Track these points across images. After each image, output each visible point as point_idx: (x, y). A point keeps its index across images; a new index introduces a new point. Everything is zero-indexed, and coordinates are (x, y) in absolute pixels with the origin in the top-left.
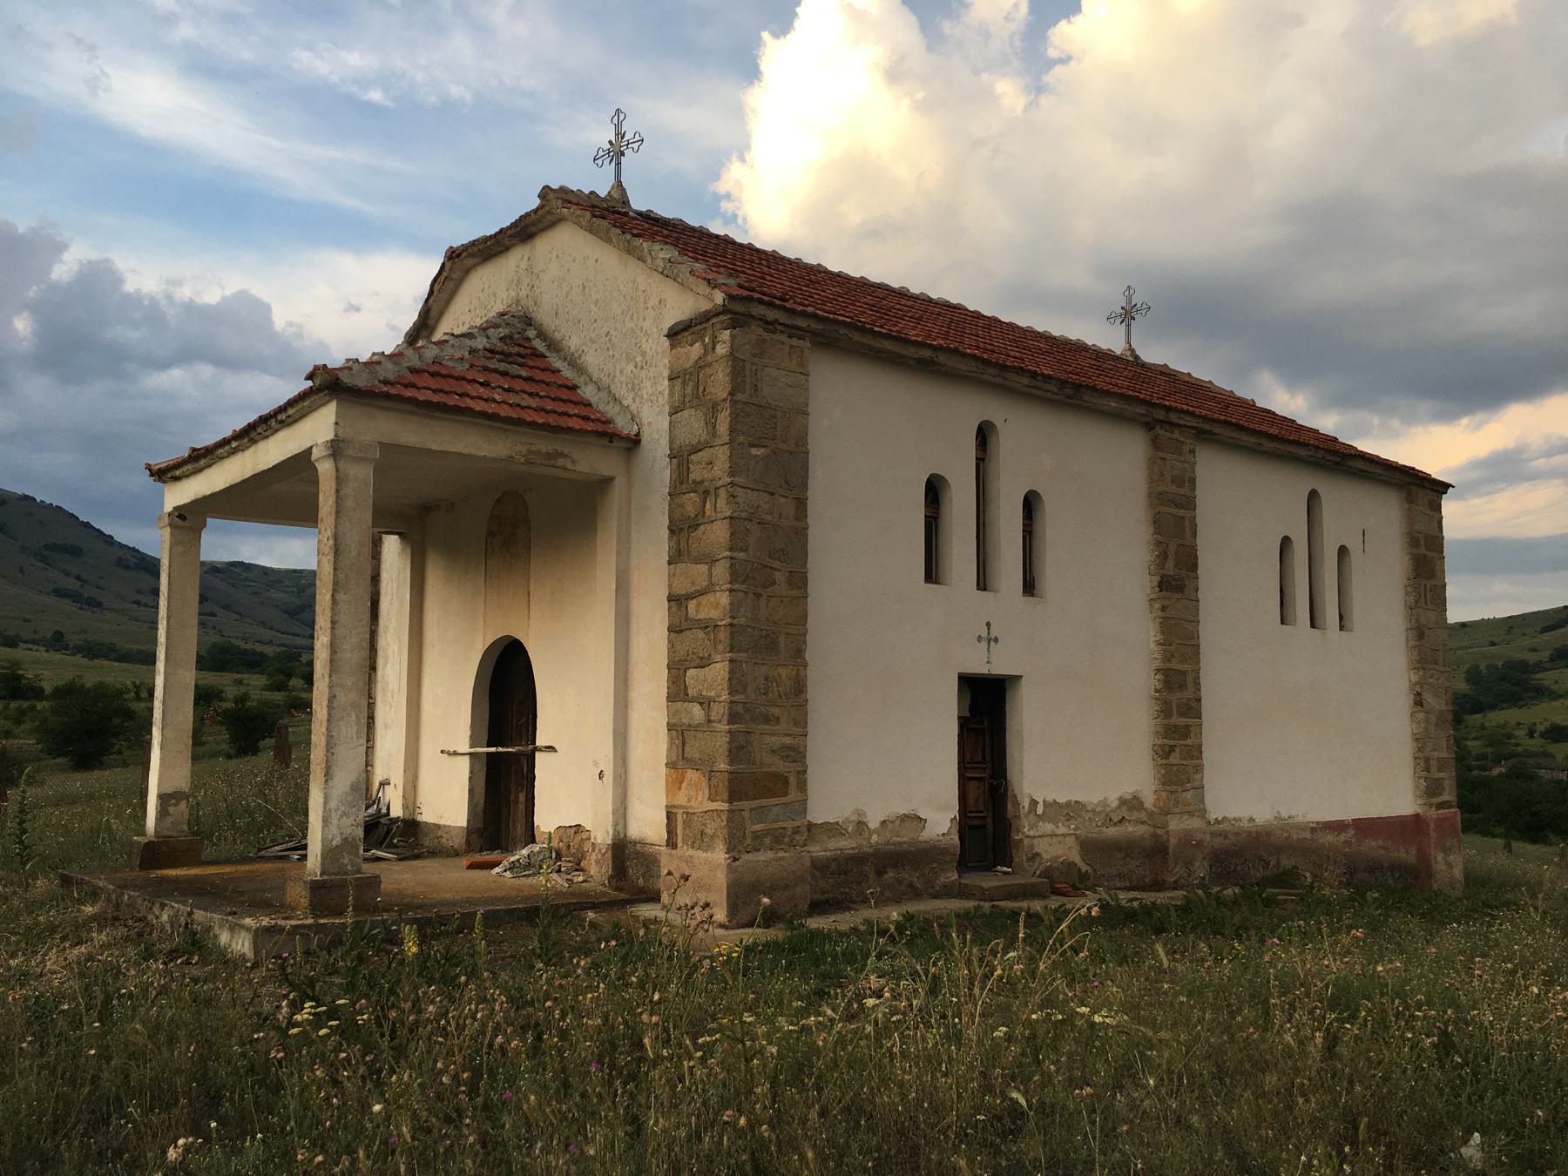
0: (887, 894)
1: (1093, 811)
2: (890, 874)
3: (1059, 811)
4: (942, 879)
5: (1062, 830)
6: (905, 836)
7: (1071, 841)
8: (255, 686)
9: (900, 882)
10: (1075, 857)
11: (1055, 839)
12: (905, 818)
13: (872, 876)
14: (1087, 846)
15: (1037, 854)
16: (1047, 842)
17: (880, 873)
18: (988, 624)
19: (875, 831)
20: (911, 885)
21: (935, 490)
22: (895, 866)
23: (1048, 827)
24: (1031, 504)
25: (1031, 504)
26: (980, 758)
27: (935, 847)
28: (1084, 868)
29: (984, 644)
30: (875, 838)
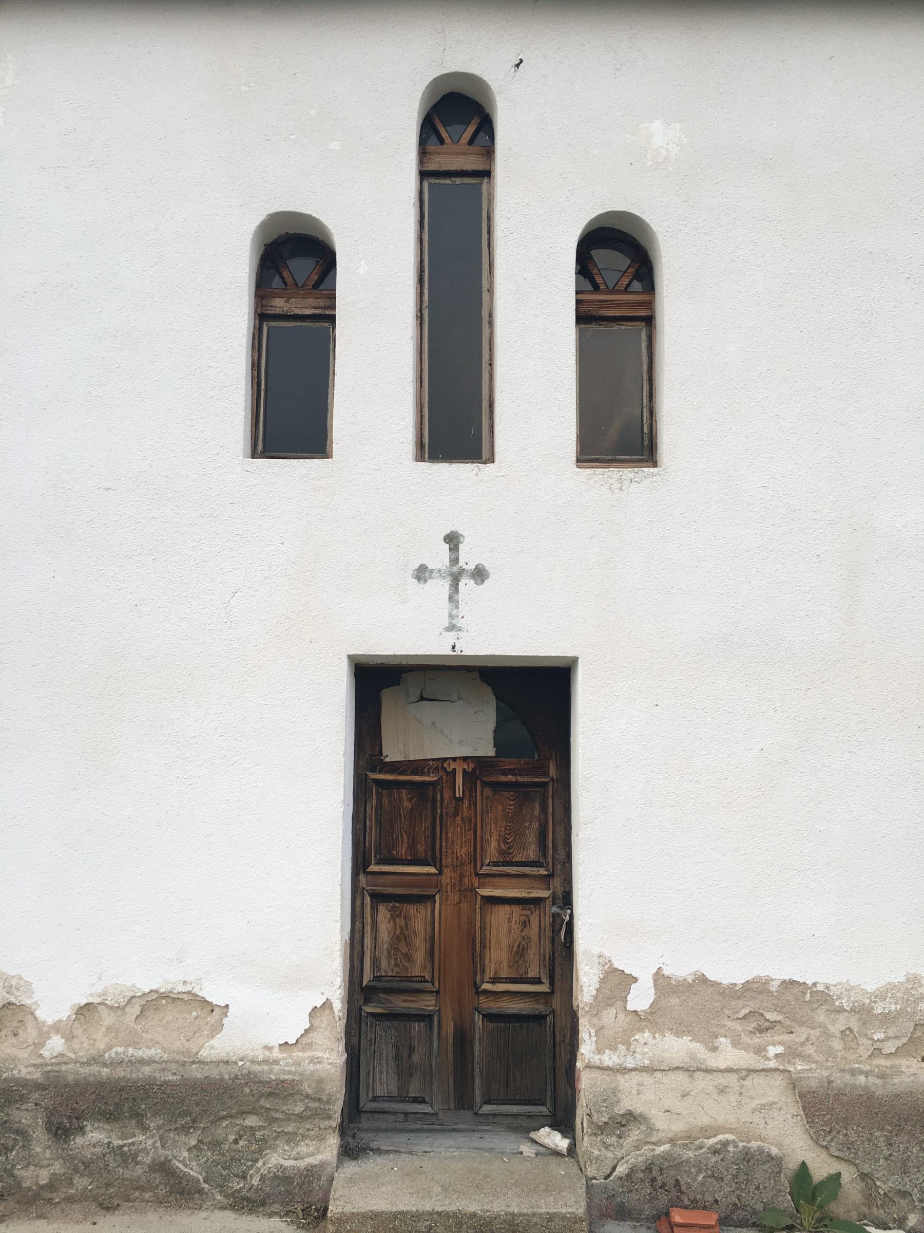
0: (81, 1182)
1: (863, 1012)
2: (95, 1136)
3: (691, 1002)
4: (279, 1159)
5: (729, 1055)
6: (155, 1048)
7: (773, 1090)
8: (737, 1038)
9: (127, 1157)
10: (792, 1141)
11: (703, 1082)
12: (155, 1002)
13: (41, 1143)
14: (823, 1109)
15: (631, 1118)
16: (656, 1083)
17: (61, 1131)
18: (453, 540)
19: (56, 1027)
20: (163, 1167)
21: (294, 260)
22: (110, 1116)
23: (677, 1047)
24: (616, 266)
25: (616, 266)
26: (532, 853)
27: (251, 1079)
28: (822, 1167)
29: (440, 588)
30: (55, 1045)
